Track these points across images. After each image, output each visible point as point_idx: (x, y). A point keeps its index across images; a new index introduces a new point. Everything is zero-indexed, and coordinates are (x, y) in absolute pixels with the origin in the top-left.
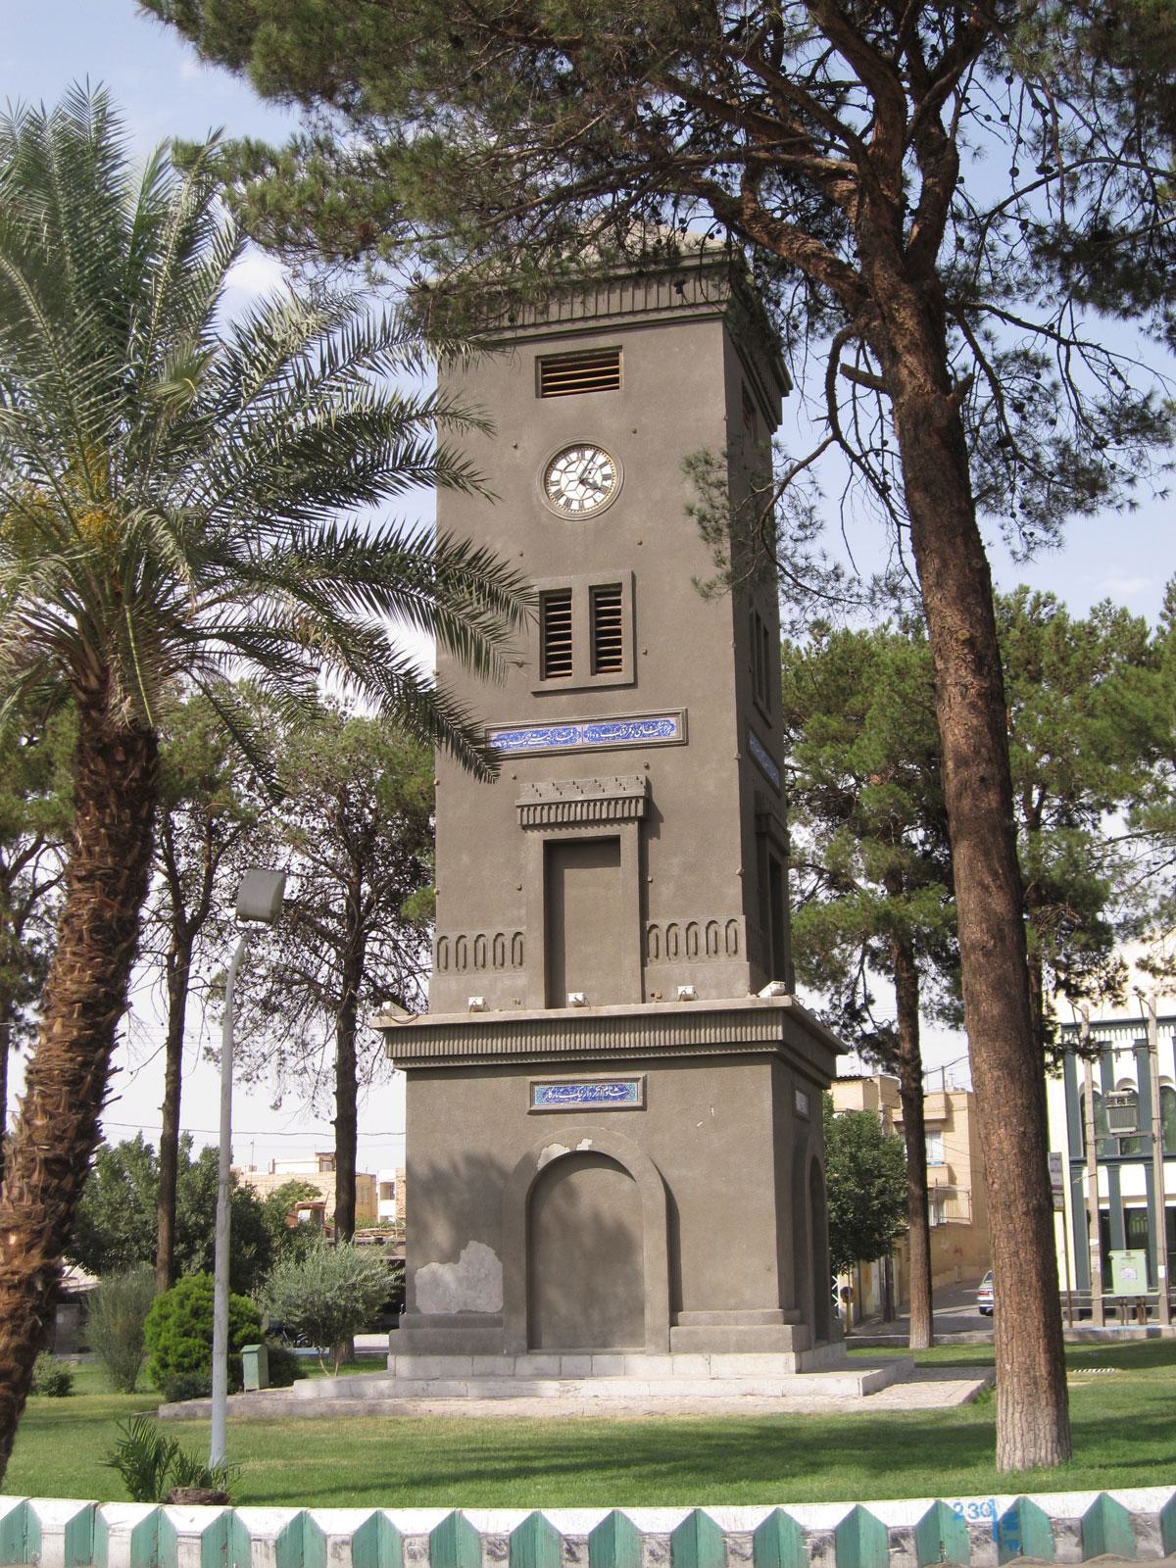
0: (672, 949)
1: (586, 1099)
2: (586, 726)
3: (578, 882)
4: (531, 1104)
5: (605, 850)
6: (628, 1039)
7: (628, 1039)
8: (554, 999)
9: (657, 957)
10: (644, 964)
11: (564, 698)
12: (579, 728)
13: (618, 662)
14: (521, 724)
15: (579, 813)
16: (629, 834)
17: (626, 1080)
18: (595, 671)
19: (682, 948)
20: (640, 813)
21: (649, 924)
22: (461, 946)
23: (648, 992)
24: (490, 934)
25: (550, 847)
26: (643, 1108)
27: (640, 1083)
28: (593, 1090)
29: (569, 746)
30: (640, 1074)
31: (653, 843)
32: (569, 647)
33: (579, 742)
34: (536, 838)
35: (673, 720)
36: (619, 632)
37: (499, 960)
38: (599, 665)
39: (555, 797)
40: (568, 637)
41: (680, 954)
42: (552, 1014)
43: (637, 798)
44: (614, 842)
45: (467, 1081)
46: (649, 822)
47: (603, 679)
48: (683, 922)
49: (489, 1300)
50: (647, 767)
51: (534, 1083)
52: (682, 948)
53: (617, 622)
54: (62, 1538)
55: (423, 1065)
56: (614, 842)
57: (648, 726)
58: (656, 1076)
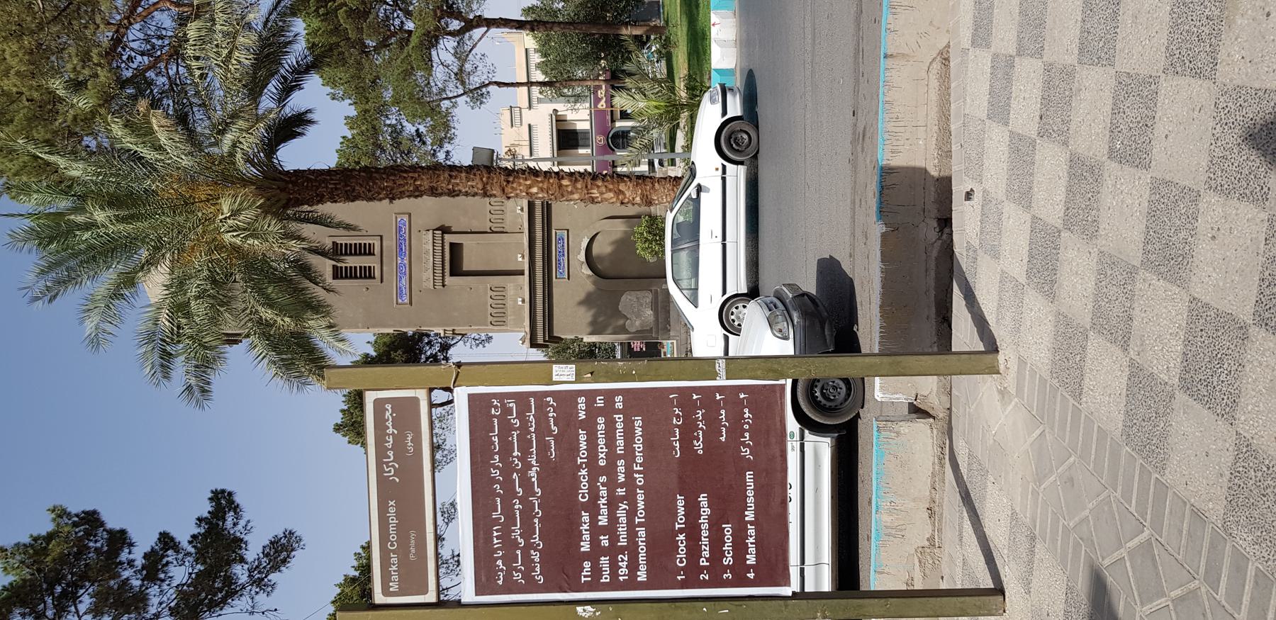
0: (501, 221)
1: (563, 255)
2: (399, 258)
3: (468, 264)
4: (565, 278)
5: (456, 249)
6: (539, 234)
7: (539, 234)
8: (522, 273)
9: (503, 228)
10: (507, 233)
11: (384, 268)
12: (399, 262)
13: (370, 244)
14: (395, 267)
15: (438, 259)
16: (449, 238)
17: (556, 237)
18: (374, 278)
19: (501, 217)
20: (440, 232)
21: (489, 231)
22: (495, 324)
23: (519, 231)
24: (490, 301)
25: (452, 274)
26: (568, 230)
27: (557, 231)
28: (560, 252)
29: (407, 266)
30: (554, 231)
31: (453, 229)
32: (360, 267)
33: (406, 262)
34: (448, 279)
35: (399, 219)
36: (355, 244)
37: (502, 298)
38: (371, 254)
39: (431, 271)
40: (355, 267)
41: (503, 208)
42: (527, 272)
43: (433, 233)
44: (451, 244)
45: (554, 308)
46: (445, 230)
47: (377, 274)
48: (489, 216)
49: (648, 297)
50: (420, 231)
51: (556, 278)
52: (501, 217)
53: (351, 245)
54: (739, 166)
55: (547, 326)
56: (451, 244)
57: (400, 230)
58: (554, 225)
